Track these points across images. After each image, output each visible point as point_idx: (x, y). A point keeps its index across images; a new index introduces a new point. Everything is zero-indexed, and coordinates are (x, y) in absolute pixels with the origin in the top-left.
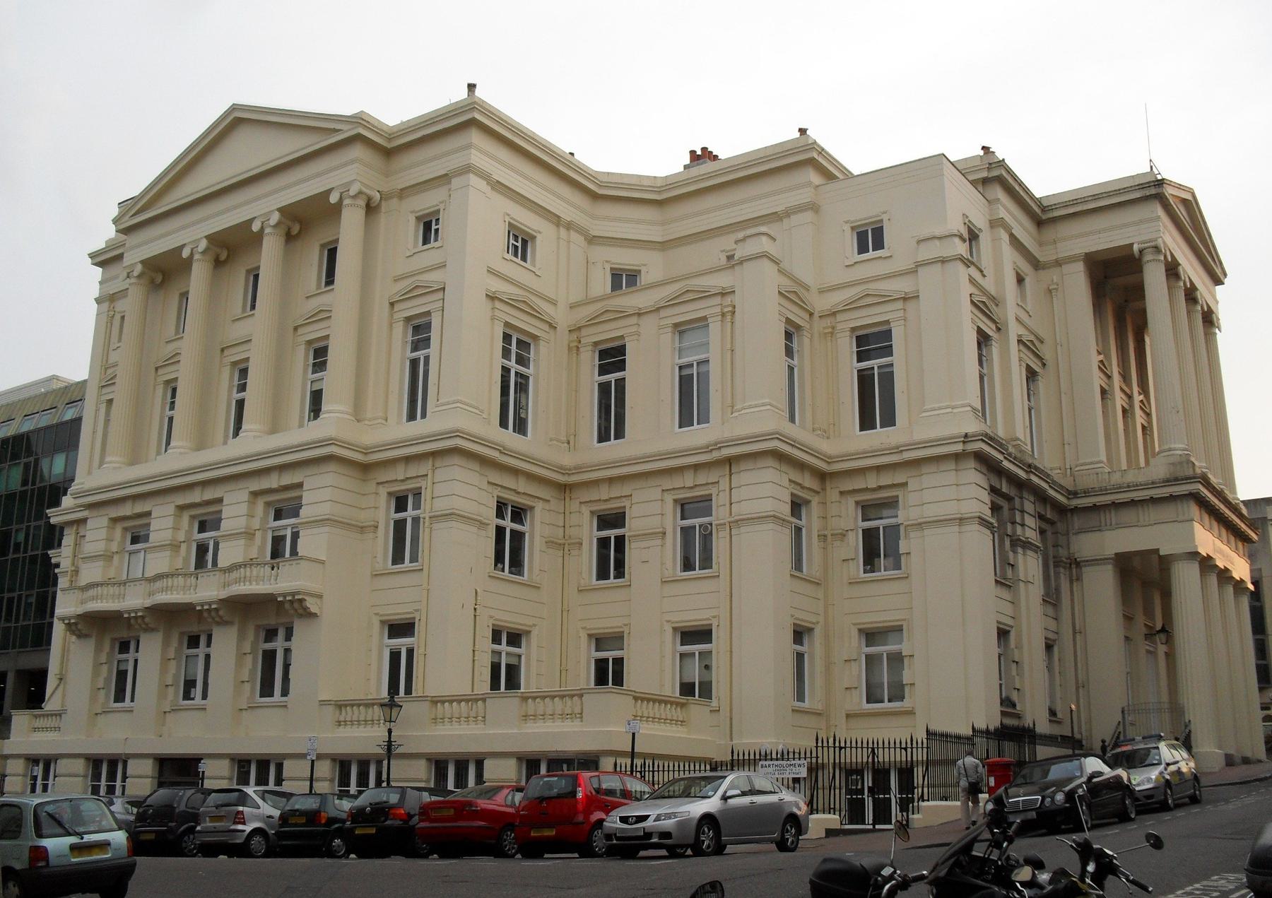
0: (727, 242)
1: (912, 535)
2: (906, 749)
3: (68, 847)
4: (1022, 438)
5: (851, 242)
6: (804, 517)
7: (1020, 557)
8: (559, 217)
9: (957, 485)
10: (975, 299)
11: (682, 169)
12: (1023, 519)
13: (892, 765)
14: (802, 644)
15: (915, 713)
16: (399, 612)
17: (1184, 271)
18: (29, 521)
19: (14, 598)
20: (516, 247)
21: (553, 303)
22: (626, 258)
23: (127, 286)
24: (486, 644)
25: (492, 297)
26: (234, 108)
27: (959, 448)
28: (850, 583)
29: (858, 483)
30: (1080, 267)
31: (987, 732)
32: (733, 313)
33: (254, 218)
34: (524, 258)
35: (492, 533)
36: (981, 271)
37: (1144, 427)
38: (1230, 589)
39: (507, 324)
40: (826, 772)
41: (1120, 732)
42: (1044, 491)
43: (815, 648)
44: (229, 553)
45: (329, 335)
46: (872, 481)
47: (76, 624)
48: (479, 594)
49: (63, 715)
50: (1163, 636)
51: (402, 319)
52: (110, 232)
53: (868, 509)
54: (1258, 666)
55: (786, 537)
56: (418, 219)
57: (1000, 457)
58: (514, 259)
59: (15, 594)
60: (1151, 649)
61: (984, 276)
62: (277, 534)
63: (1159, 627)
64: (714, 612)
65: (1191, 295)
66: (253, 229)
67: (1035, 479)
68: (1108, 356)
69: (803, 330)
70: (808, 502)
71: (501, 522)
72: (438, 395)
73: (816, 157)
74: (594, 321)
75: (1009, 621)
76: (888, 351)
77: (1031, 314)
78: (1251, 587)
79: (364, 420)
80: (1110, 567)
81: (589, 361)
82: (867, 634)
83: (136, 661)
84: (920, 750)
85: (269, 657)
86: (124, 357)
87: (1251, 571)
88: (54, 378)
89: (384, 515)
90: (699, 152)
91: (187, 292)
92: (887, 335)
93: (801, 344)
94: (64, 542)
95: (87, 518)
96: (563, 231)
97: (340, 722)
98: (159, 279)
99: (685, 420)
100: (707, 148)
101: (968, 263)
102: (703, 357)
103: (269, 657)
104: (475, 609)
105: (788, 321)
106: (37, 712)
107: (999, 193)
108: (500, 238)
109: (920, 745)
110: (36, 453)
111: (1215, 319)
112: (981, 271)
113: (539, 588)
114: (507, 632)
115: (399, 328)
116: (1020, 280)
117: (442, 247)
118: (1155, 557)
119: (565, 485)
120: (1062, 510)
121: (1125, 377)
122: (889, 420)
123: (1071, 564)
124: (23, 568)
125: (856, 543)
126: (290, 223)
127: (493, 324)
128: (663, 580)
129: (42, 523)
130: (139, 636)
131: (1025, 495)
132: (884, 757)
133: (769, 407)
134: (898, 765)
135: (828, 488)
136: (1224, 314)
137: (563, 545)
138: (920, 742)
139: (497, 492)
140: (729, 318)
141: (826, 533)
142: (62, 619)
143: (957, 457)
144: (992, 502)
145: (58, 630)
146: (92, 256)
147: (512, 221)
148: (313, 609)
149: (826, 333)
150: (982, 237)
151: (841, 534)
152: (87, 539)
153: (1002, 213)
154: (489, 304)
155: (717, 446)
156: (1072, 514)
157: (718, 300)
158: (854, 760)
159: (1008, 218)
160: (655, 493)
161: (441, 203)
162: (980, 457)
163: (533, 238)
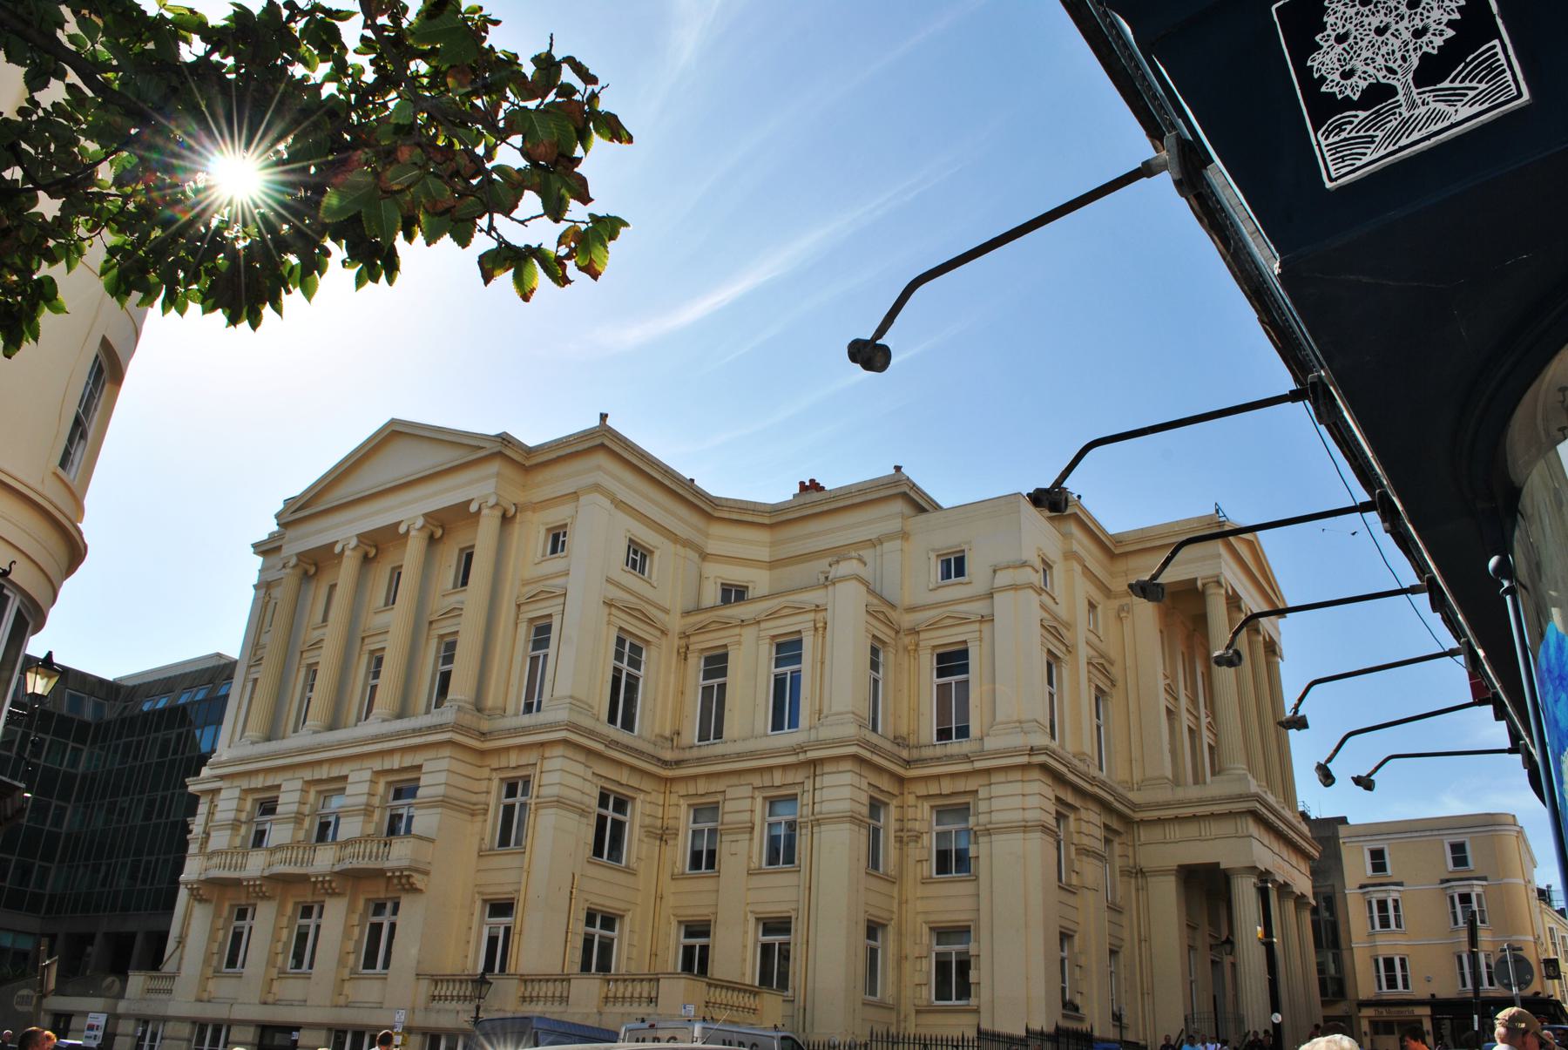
0: (822, 564)
1: (981, 839)
5: (936, 569)
6: (882, 820)
9: (1023, 795)
10: (1046, 623)
11: (791, 498)
16: (500, 891)
18: (174, 788)
22: (737, 575)
23: (283, 576)
24: (580, 928)
25: (609, 604)
26: (393, 422)
27: (1024, 760)
31: (1042, 1033)
33: (337, 542)
34: (642, 571)
35: (593, 821)
38: (1290, 905)
39: (621, 629)
43: (888, 946)
47: (198, 889)
50: (1228, 947)
52: (273, 527)
54: (1319, 979)
55: (863, 837)
56: (548, 530)
58: (633, 571)
59: (153, 858)
62: (394, 812)
63: (1224, 938)
68: (1175, 679)
71: (604, 812)
76: (964, 669)
78: (1314, 903)
80: (1173, 878)
81: (696, 664)
82: (938, 934)
83: (251, 928)
85: (376, 929)
86: (273, 641)
87: (1313, 887)
88: (219, 655)
89: (495, 799)
90: (807, 484)
91: (335, 585)
92: (964, 654)
93: (886, 657)
94: (199, 811)
95: (221, 789)
99: (777, 725)
101: (1040, 591)
103: (376, 929)
104: (571, 892)
105: (874, 636)
106: (154, 974)
115: (523, 627)
116: (1092, 606)
121: (1194, 701)
123: (1137, 874)
130: (324, 902)
135: (906, 793)
142: (186, 884)
144: (1057, 812)
145: (183, 894)
146: (255, 546)
148: (419, 885)
150: (1055, 567)
151: (916, 836)
152: (219, 809)
153: (1076, 547)
154: (606, 610)
156: (1138, 827)
157: (811, 616)
159: (1082, 553)
160: (747, 791)
162: (1044, 767)
163: (652, 552)
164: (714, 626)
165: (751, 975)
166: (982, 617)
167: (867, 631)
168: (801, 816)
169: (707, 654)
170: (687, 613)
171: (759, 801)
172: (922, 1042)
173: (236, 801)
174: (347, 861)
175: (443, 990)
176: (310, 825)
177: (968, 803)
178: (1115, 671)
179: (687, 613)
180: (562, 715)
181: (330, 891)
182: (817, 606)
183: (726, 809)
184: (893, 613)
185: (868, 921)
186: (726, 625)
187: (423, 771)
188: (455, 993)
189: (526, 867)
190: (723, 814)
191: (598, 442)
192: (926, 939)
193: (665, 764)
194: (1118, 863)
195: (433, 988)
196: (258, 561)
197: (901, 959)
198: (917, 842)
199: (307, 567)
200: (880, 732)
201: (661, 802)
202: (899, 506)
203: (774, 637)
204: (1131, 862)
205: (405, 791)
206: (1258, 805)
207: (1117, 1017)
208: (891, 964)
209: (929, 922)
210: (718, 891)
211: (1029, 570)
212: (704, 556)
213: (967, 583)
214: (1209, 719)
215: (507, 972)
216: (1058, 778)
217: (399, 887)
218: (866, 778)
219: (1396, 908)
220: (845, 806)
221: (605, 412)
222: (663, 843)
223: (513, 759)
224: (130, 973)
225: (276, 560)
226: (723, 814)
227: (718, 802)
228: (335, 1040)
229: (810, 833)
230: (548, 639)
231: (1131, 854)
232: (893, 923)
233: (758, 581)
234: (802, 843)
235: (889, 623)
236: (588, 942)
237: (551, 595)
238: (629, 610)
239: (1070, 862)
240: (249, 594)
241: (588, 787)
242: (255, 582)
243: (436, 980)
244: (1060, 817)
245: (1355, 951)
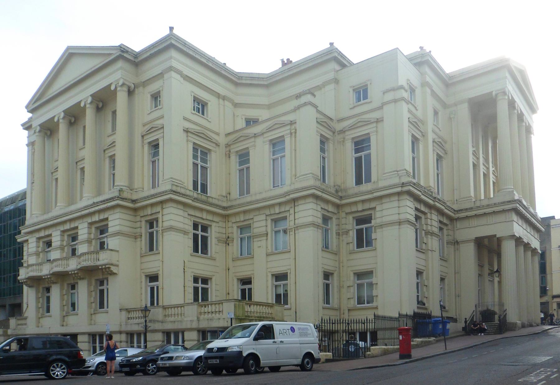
1: (378, 230)
2: (364, 324)
3: (462, 328)
6: (329, 225)
7: (430, 240)
8: (219, 94)
12: (431, 222)
13: (358, 330)
14: (328, 280)
15: (378, 308)
17: (526, 118)
20: (199, 108)
21: (218, 134)
24: (191, 285)
25: (186, 131)
26: (69, 48)
27: (399, 189)
28: (350, 253)
29: (354, 209)
30: (466, 105)
31: (407, 315)
32: (296, 133)
33: (81, 101)
34: (203, 114)
35: (191, 236)
36: (415, 108)
37: (484, 174)
39: (194, 143)
40: (339, 334)
41: (474, 315)
43: (334, 282)
44: (82, 249)
46: (277, 210)
48: (186, 262)
50: (497, 274)
53: (360, 221)
56: (152, 96)
57: (443, 208)
58: (198, 114)
60: (491, 280)
61: (417, 110)
63: (495, 270)
64: (288, 267)
65: (521, 117)
70: (331, 218)
73: (337, 56)
74: (236, 141)
75: (423, 268)
77: (441, 129)
78: (540, 252)
79: (134, 189)
81: (234, 159)
84: (371, 324)
89: (144, 230)
90: (286, 62)
92: (368, 140)
96: (221, 101)
97: (129, 318)
98: (49, 133)
101: (408, 102)
102: (283, 154)
103: (102, 292)
104: (184, 269)
107: (427, 69)
108: (189, 104)
109: (371, 322)
111: (532, 130)
112: (415, 108)
113: (215, 260)
114: (201, 279)
115: (146, 147)
116: (436, 113)
117: (162, 108)
118: (495, 239)
119: (226, 215)
120: (451, 219)
121: (486, 160)
122: (369, 180)
123: (455, 243)
125: (352, 236)
126: (97, 102)
127: (188, 144)
131: (433, 212)
132: (354, 327)
133: (311, 175)
134: (371, 330)
135: (340, 212)
136: (536, 127)
138: (371, 320)
139: (193, 219)
140: (294, 135)
141: (339, 231)
143: (399, 194)
146: (23, 125)
147: (195, 95)
148: (115, 271)
149: (340, 142)
151: (346, 232)
153: (428, 79)
155: (287, 194)
156: (456, 221)
157: (288, 127)
158: (331, 329)
160: (263, 217)
161: (160, 87)
163: (207, 104)
164: (242, 139)
165: (271, 299)
167: (317, 131)
171: (269, 222)
172: (347, 322)
173: (35, 243)
174: (82, 264)
175: (132, 315)
177: (372, 214)
178: (447, 147)
180: (168, 187)
182: (291, 121)
185: (324, 271)
186: (247, 137)
187: (109, 220)
190: (253, 229)
193: (224, 208)
194: (446, 238)
195: (128, 314)
196: (26, 132)
197: (340, 287)
198: (347, 234)
202: (334, 66)
205: (103, 230)
206: (518, 205)
207: (443, 307)
208: (336, 290)
209: (353, 271)
211: (403, 91)
213: (369, 103)
214: (494, 169)
215: (159, 305)
216: (417, 199)
220: (310, 219)
221: (172, 26)
222: (227, 245)
223: (149, 211)
226: (253, 229)
227: (251, 224)
228: (92, 338)
229: (294, 234)
232: (336, 272)
235: (329, 128)
236: (196, 289)
239: (422, 238)
240: (26, 149)
241: (187, 221)
242: (27, 143)
243: (128, 311)
244: (417, 218)
245: (553, 275)
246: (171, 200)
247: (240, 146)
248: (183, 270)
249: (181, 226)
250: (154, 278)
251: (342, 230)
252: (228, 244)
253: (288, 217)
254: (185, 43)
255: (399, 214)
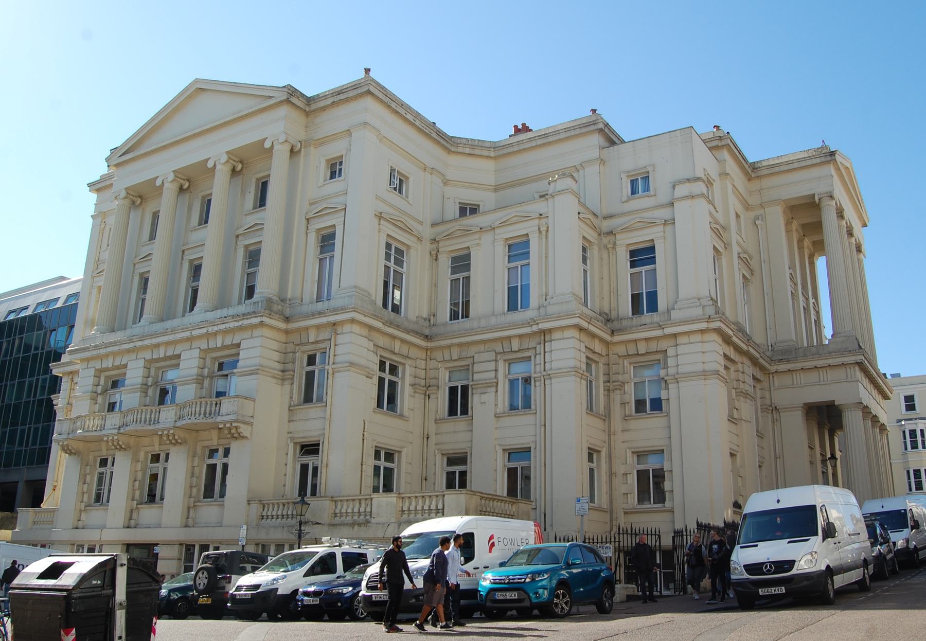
4: (741, 322)
9: (703, 353)
13: (658, 548)
19: (25, 429)
21: (421, 223)
24: (371, 462)
25: (380, 217)
26: (197, 81)
27: (704, 325)
35: (376, 381)
42: (757, 359)
45: (261, 241)
49: (56, 512)
51: (314, 230)
56: (328, 161)
61: (717, 212)
66: (208, 166)
67: (751, 350)
69: (594, 245)
72: (340, 283)
76: (652, 260)
77: (744, 240)
80: (800, 413)
81: (445, 263)
83: (112, 473)
90: (520, 127)
92: (652, 249)
100: (525, 124)
104: (363, 435)
107: (725, 155)
110: (45, 327)
116: (738, 216)
123: (772, 410)
124: (33, 408)
128: (496, 416)
129: (48, 376)
134: (626, 549)
137: (426, 389)
138: (692, 531)
146: (90, 185)
157: (536, 222)
158: (626, 545)
162: (718, 331)
166: (665, 221)
168: (535, 373)
169: (454, 255)
170: (434, 225)
176: (154, 393)
178: (754, 264)
179: (434, 225)
181: (173, 442)
183: (475, 370)
184: (596, 220)
186: (467, 232)
188: (269, 513)
189: (328, 416)
191: (365, 89)
192: (629, 460)
196: (93, 197)
199: (135, 199)
200: (589, 307)
201: (423, 367)
203: (507, 239)
204: (768, 402)
209: (631, 448)
210: (472, 431)
212: (446, 183)
217: (229, 436)
218: (584, 343)
219: (923, 435)
220: (572, 363)
224: (19, 510)
225: (108, 194)
228: (186, 553)
229: (543, 385)
230: (334, 244)
231: (768, 396)
232: (604, 449)
233: (485, 199)
234: (536, 392)
237: (334, 211)
238: (394, 223)
246: (353, 321)
247: (458, 245)
248: (362, 435)
249: (363, 362)
250: (311, 449)
251: (613, 382)
252: (429, 395)
253: (533, 358)
254: (382, 89)
255: (703, 363)
